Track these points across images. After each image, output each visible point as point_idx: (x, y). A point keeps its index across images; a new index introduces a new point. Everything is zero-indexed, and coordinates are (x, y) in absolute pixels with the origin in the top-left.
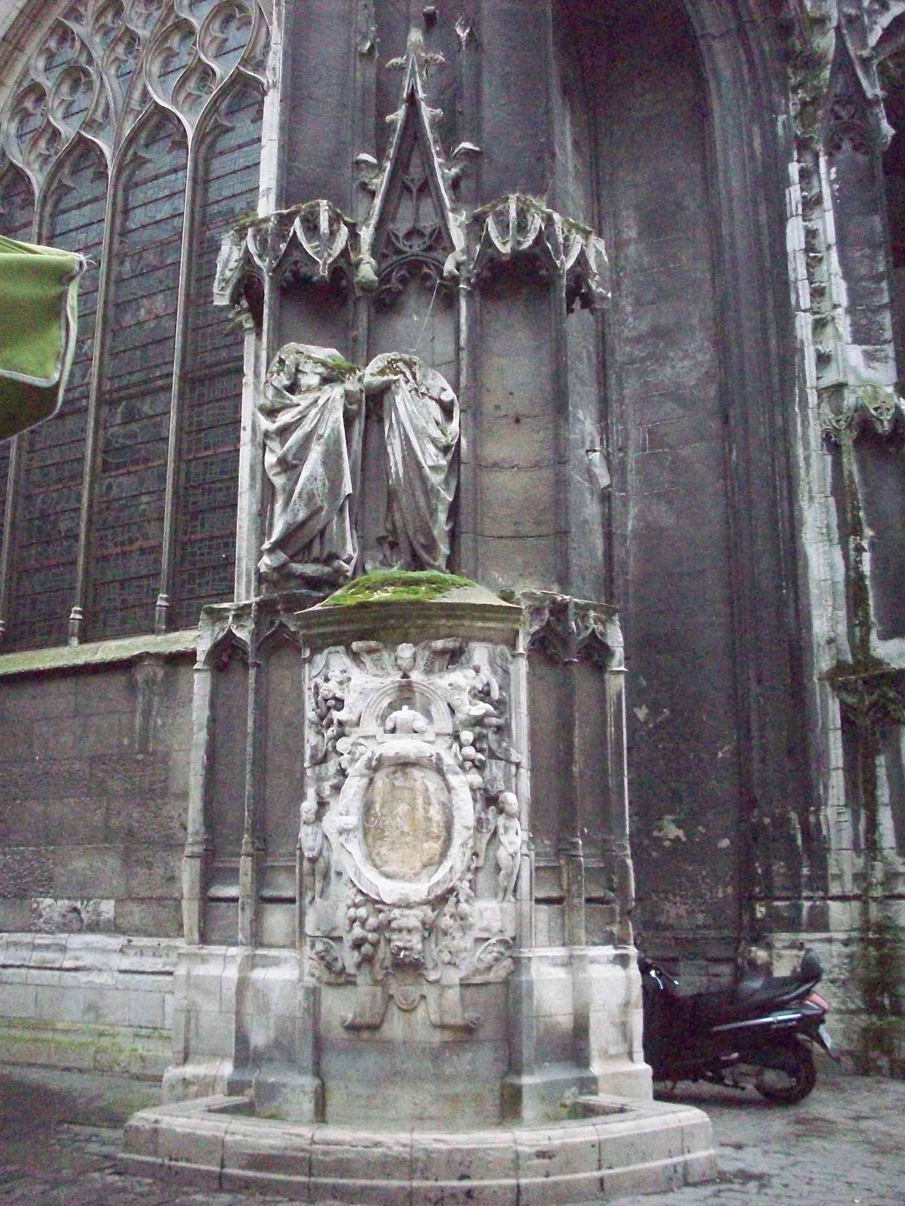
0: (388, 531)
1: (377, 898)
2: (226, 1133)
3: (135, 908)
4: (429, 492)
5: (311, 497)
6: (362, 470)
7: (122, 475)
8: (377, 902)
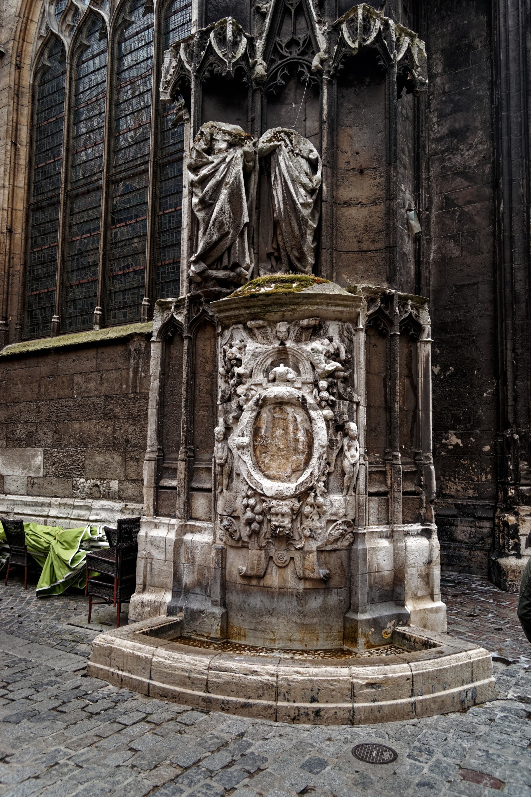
0: (274, 248)
1: (262, 492)
2: (153, 655)
3: (128, 485)
4: (302, 221)
5: (222, 224)
6: (257, 208)
7: (123, 226)
8: (262, 495)
